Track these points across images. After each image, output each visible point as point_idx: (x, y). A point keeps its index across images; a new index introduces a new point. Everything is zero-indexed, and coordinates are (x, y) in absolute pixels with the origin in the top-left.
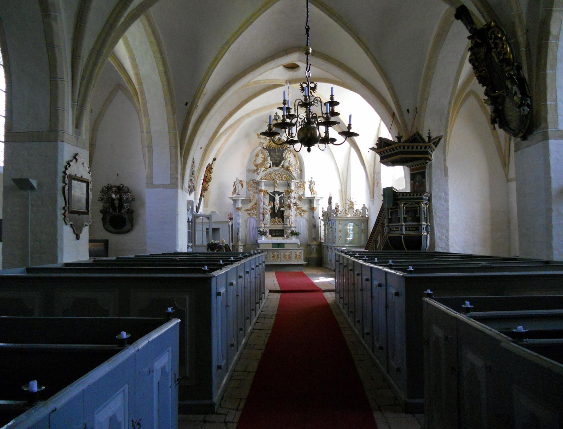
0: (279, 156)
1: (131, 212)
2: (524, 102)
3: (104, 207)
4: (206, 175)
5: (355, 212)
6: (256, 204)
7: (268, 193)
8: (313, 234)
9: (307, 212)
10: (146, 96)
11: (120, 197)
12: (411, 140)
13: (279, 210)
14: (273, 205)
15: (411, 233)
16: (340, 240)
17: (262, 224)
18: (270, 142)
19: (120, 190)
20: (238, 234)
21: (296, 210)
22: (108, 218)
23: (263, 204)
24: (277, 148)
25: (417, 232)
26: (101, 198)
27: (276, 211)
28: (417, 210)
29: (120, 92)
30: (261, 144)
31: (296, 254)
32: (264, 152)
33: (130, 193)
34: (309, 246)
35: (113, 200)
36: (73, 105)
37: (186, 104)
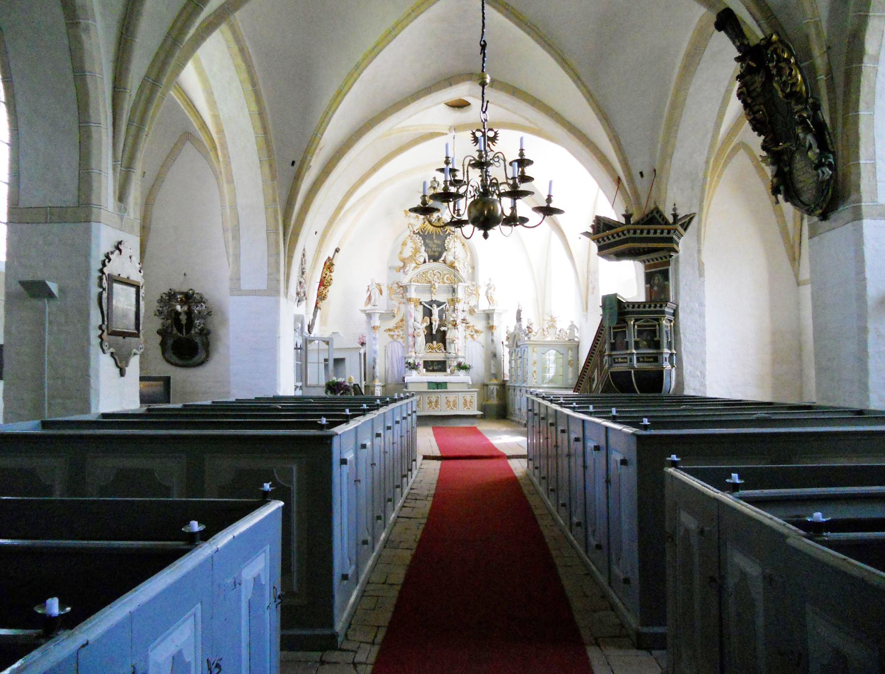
0: (438, 246)
1: (205, 333)
2: (823, 160)
3: (163, 325)
4: (324, 275)
5: (558, 332)
6: (402, 320)
7: (421, 303)
8: (492, 367)
9: (482, 334)
10: (230, 150)
11: (188, 309)
12: (645, 220)
13: (438, 331)
14: (429, 322)
15: (646, 366)
16: (535, 377)
17: (411, 352)
18: (425, 222)
19: (188, 298)
20: (374, 368)
21: (465, 330)
22: (170, 342)
23: (413, 320)
24: (436, 233)
25: (656, 364)
26: (158, 310)
27: (434, 332)
28: (655, 330)
29: (188, 144)
30: (410, 226)
31: (465, 400)
32: (415, 239)
33: (204, 303)
34: (485, 387)
35: (178, 314)
36: (115, 165)
37: (293, 163)
